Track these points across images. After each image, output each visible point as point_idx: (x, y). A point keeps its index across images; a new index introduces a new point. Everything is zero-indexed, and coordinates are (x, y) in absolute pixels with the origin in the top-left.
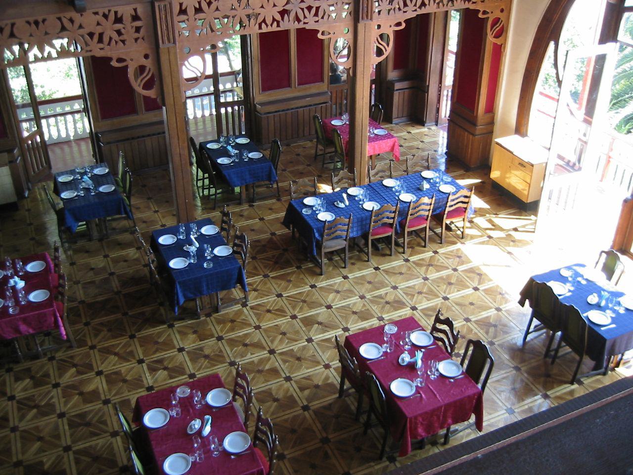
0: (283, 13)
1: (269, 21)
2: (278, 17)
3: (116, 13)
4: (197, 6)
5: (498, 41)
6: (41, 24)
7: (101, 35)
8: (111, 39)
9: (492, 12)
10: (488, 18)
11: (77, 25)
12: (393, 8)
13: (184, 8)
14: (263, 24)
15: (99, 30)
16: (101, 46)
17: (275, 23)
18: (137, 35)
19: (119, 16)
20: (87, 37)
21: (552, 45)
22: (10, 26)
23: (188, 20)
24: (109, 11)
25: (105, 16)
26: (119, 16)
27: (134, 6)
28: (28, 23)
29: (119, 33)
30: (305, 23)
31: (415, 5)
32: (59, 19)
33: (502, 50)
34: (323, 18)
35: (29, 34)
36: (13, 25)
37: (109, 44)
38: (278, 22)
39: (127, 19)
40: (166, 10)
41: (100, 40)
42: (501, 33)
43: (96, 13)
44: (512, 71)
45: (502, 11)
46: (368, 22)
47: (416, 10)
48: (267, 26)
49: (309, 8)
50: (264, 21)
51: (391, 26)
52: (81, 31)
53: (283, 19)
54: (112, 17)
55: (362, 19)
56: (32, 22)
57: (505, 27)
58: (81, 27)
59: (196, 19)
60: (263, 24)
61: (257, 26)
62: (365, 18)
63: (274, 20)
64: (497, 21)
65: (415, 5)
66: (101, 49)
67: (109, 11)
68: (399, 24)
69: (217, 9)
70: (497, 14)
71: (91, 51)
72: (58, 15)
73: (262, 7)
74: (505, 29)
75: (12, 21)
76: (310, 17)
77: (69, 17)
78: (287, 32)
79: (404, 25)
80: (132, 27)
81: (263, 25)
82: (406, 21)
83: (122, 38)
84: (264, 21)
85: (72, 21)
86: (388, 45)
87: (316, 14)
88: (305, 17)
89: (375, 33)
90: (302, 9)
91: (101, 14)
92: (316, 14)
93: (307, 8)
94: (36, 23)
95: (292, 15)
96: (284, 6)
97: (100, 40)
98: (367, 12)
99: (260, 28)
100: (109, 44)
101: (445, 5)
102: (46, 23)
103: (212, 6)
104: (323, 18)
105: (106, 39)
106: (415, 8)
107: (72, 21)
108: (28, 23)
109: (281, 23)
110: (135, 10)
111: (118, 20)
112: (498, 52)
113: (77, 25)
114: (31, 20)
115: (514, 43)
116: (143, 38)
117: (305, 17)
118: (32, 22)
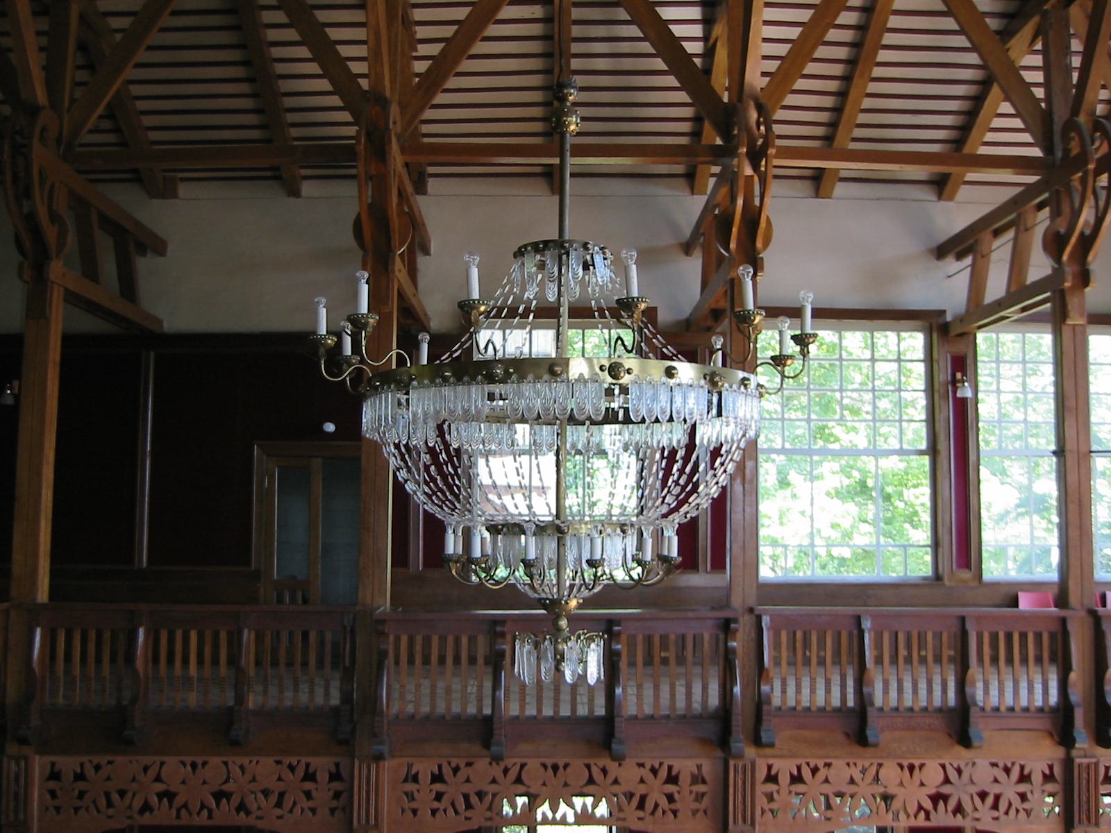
0: (936, 798)
1: (912, 809)
2: (928, 804)
3: (670, 768)
4: (795, 773)
6: (916, 771)
7: (997, 798)
8: (656, 805)
15: (995, 789)
16: (641, 814)
17: (205, 812)
18: (436, 805)
19: (674, 773)
22: (518, 766)
24: (661, 764)
25: (654, 771)
26: (674, 773)
27: (798, 761)
28: (544, 766)
29: (670, 798)
32: (588, 766)
34: (291, 811)
36: (523, 766)
37: (653, 813)
39: (425, 778)
41: (641, 806)
43: (641, 765)
48: (190, 814)
50: (185, 806)
52: (252, 786)
53: (935, 809)
54: (663, 773)
58: (616, 782)
63: (920, 808)
65: (130, 807)
66: (639, 819)
67: (661, 764)
72: (587, 761)
73: (901, 784)
75: (524, 760)
81: (183, 811)
83: (1027, 805)
85: (604, 771)
87: (995, 807)
91: (648, 767)
92: (995, 807)
93: (625, 795)
94: (555, 768)
95: (952, 804)
97: (641, 806)
99: (178, 817)
100: (653, 813)
103: (459, 774)
104: (291, 811)
105: (649, 805)
107: (604, 771)
108: (544, 766)
109: (933, 814)
110: (337, 765)
111: (672, 779)
113: (610, 779)
114: (549, 762)
116: (705, 812)
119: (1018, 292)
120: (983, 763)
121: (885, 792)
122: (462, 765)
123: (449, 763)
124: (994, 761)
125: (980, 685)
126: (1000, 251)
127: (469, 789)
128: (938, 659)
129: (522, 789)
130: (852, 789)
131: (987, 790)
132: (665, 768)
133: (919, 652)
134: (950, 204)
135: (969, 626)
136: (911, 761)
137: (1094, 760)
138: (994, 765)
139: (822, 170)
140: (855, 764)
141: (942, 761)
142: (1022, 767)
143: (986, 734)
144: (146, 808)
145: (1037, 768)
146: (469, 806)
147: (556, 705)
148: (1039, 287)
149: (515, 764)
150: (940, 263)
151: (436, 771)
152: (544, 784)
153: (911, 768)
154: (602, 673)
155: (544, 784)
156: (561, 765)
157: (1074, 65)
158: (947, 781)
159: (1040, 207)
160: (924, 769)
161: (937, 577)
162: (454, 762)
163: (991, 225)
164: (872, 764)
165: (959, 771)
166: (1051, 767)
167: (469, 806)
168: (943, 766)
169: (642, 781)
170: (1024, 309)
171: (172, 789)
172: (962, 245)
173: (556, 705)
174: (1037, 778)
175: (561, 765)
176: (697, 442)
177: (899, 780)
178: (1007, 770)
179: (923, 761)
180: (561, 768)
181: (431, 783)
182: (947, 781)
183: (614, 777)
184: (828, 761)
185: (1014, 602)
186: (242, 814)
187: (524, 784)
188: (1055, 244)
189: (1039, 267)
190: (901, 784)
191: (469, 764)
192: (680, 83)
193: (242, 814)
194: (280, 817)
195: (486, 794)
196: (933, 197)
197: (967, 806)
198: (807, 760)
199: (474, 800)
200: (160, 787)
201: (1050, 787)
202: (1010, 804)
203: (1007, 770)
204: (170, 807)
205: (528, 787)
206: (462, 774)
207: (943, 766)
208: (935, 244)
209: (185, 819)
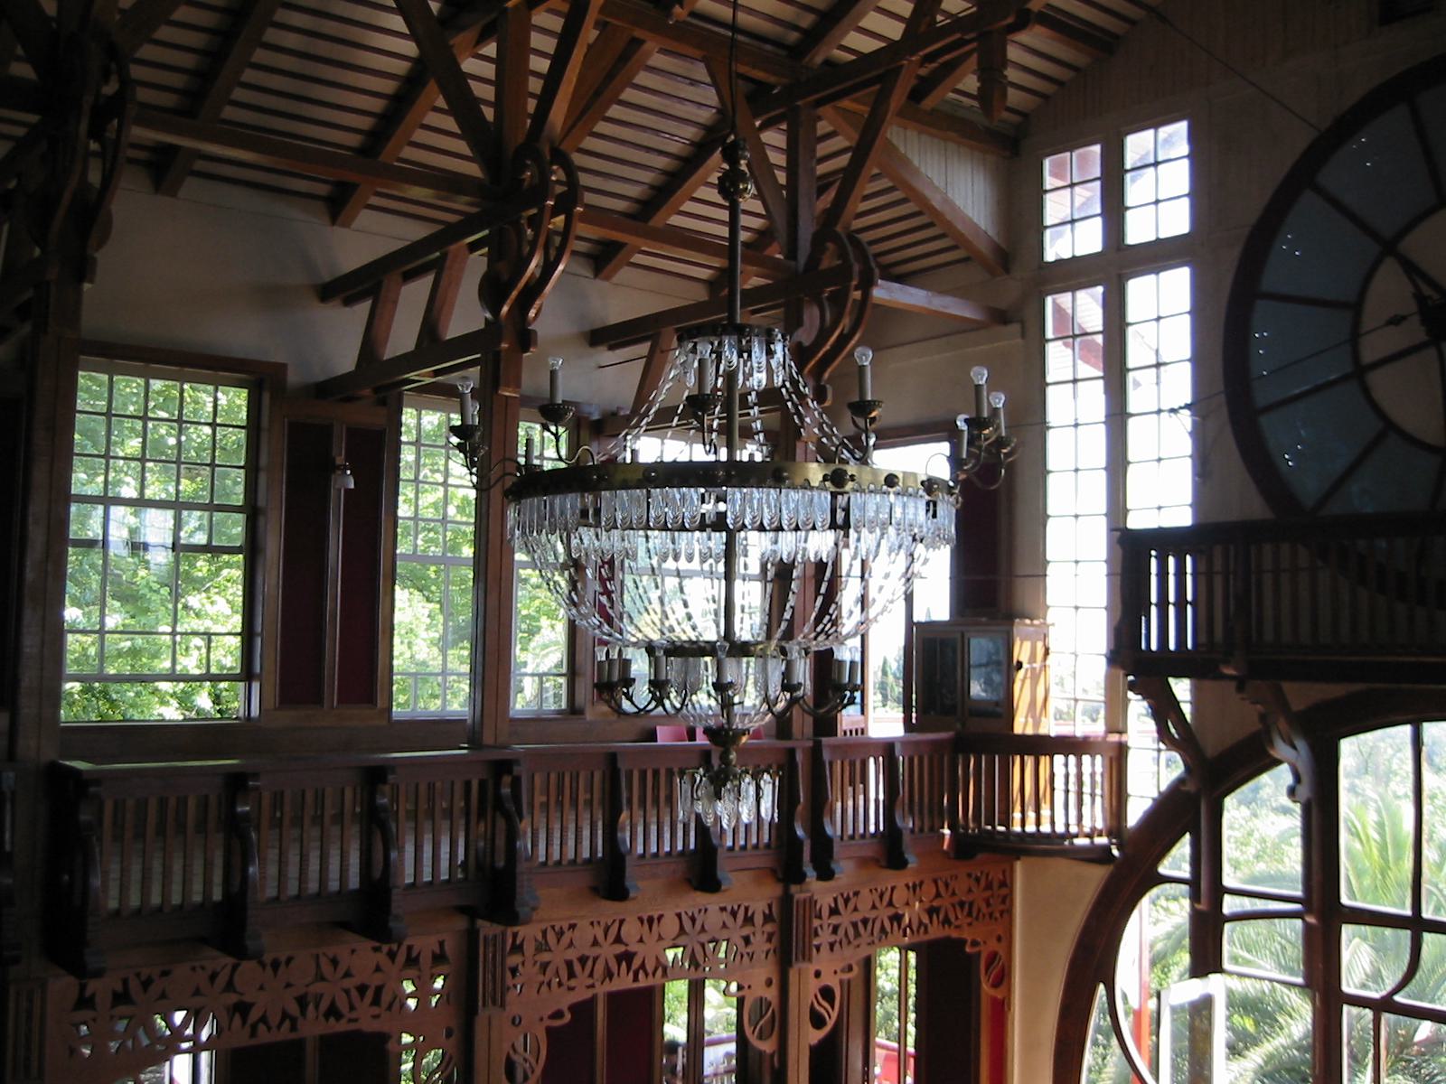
1: (274, 1019)
2: (294, 1009)
3: (747, 909)
5: (999, 994)
6: (282, 968)
8: (979, 910)
9: (985, 943)
10: (979, 953)
11: (342, 968)
12: (546, 980)
13: (414, 954)
14: (641, 972)
15: (376, 980)
17: (287, 1024)
19: (414, 954)
20: (354, 993)
21: (1101, 989)
22: (617, 924)
23: (94, 1020)
24: (739, 906)
30: (350, 1020)
31: (591, 975)
33: (1006, 1009)
35: (258, 986)
37: (977, 918)
38: (294, 1021)
40: (495, 945)
41: (376, 1001)
42: (1003, 979)
44: (1030, 1047)
45: (999, 939)
46: (803, 965)
47: (592, 986)
48: (269, 1029)
49: (362, 989)
50: (263, 1019)
51: (835, 972)
53: (931, 922)
55: (484, 1005)
56: (645, 918)
57: (1006, 968)
58: (347, 974)
59: (112, 1017)
60: (641, 972)
61: (248, 1029)
62: (800, 957)
64: (993, 957)
65: (591, 975)
67: (739, 906)
68: (558, 1015)
69: (571, 944)
70: (993, 945)
71: (356, 1020)
73: (641, 940)
74: (1006, 972)
76: (364, 1009)
77: (331, 955)
78: (299, 1045)
79: (568, 1017)
80: (829, 925)
82: (572, 1008)
83: (749, 950)
84: (643, 966)
85: (334, 962)
86: (833, 1008)
88: (352, 1008)
89: (813, 986)
90: (347, 992)
94: (651, 920)
96: (674, 939)
98: (494, 989)
99: (253, 1033)
101: (651, 975)
102: (292, 964)
106: (590, 981)
107: (334, 962)
108: (969, 875)
109: (300, 1022)
110: (441, 944)
112: (1001, 1010)
115: (1025, 997)
117: (352, 1008)
118: (645, 918)
119: (432, 346)
120: (713, 908)
121: (626, 951)
122: (565, 928)
123: (138, 975)
124: (722, 905)
125: (409, 849)
126: (413, 297)
127: (572, 955)
128: (339, 818)
129: (664, 943)
130: (725, 934)
131: (867, 916)
132: (742, 908)
133: (548, 800)
134: (605, 284)
135: (623, 766)
136: (650, 914)
137: (809, 895)
138: (723, 909)
139: (174, 149)
140: (599, 923)
141: (678, 911)
142: (747, 909)
143: (640, 884)
144: (609, 974)
145: (759, 908)
146: (571, 975)
147: (1038, 823)
148: (465, 343)
149: (226, 965)
150: (592, 350)
151: (119, 988)
152: (261, 988)
153: (275, 965)
154: (776, 815)
155: (261, 988)
156: (656, 917)
157: (1057, 248)
158: (938, 895)
159: (473, 247)
160: (663, 921)
161: (574, 710)
162: (145, 972)
163: (405, 263)
164: (614, 921)
165: (693, 920)
166: (770, 906)
167: (571, 975)
168: (679, 916)
169: (378, 969)
170: (437, 373)
171: (247, 999)
172: (367, 285)
173: (1038, 823)
174: (759, 919)
175: (283, 959)
176: (723, 582)
177: (638, 937)
178: (734, 914)
179: (661, 913)
180: (656, 921)
181: (113, 1007)
182: (321, 978)
183: (345, 969)
184: (572, 922)
185: (652, 736)
186: (332, 1020)
187: (235, 992)
188: (492, 291)
189: (466, 317)
190: (641, 940)
191: (165, 974)
192: (460, 128)
193: (332, 1020)
194: (376, 1017)
195: (588, 958)
196: (590, 274)
197: (342, 1005)
198: (553, 923)
199: (577, 967)
200: (620, 949)
201: (769, 928)
202: (979, 910)
203: (734, 914)
204: (244, 1021)
205: (242, 994)
206: (565, 939)
207: (679, 916)
208: (587, 328)
209: (264, 1036)
